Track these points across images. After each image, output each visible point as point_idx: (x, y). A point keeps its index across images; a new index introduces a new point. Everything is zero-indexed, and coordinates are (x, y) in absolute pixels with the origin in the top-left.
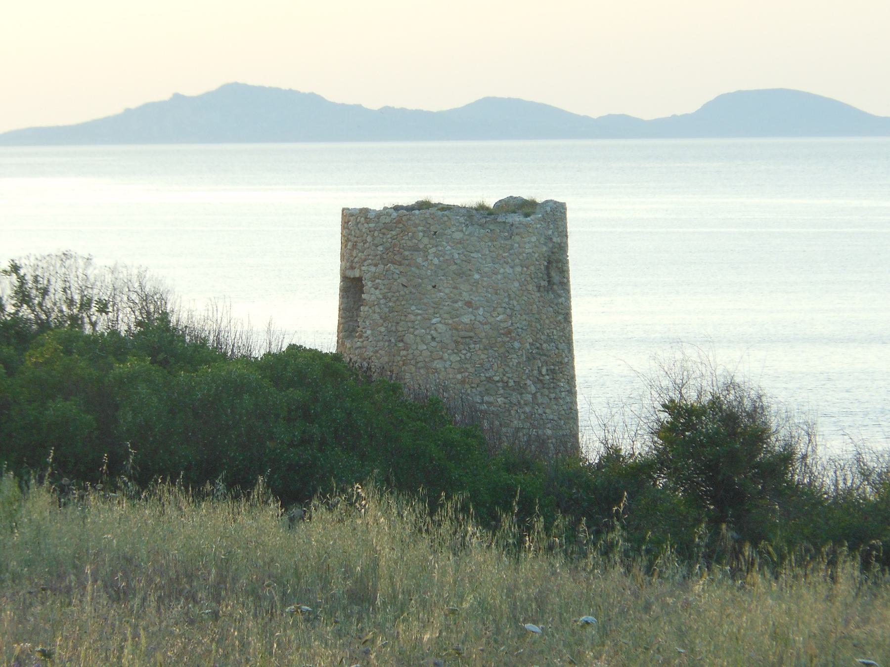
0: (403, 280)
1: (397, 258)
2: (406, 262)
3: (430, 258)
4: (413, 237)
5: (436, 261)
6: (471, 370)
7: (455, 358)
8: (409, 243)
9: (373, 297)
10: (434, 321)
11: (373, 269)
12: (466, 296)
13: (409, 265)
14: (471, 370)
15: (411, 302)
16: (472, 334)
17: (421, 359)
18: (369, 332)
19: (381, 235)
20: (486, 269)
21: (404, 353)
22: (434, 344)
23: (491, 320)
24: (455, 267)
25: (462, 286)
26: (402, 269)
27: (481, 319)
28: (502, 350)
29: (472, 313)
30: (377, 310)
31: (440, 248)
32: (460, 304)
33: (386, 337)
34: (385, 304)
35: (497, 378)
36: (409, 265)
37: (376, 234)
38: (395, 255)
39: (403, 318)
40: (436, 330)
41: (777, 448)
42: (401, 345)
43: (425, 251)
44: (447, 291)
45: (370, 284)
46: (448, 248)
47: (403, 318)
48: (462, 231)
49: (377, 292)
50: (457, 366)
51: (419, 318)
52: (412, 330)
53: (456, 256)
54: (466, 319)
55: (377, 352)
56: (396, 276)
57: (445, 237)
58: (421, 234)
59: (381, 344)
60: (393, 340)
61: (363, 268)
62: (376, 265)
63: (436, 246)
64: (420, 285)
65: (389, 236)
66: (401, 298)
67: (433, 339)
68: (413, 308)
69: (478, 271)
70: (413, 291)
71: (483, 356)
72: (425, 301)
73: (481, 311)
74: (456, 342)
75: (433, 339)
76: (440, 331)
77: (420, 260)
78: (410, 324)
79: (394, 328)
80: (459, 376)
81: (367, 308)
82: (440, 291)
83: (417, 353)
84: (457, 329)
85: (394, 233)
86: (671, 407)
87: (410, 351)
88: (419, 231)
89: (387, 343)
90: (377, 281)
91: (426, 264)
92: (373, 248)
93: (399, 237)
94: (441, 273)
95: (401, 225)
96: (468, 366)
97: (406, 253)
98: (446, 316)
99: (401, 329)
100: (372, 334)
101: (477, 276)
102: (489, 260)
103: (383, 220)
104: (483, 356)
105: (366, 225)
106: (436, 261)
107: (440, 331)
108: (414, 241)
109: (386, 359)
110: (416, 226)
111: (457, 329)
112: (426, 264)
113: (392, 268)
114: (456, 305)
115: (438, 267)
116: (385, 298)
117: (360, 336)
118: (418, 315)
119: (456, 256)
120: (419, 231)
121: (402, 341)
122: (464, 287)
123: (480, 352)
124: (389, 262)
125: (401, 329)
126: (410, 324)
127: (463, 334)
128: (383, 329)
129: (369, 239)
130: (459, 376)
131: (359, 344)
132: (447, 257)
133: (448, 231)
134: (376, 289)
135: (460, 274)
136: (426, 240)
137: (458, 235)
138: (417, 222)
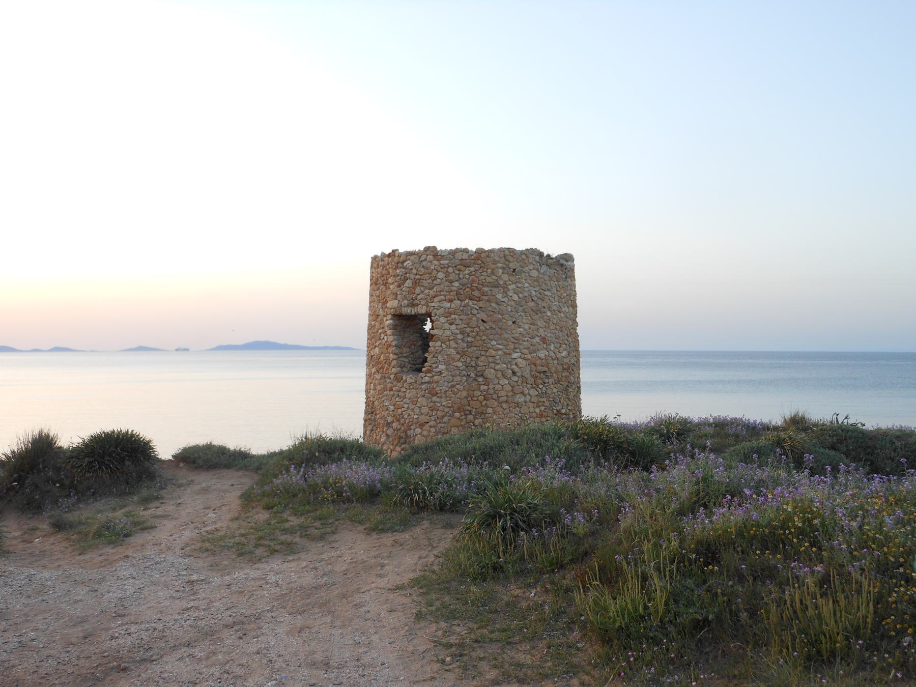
0: (483, 316)
1: (476, 293)
2: (486, 298)
3: (510, 294)
4: (493, 273)
5: (516, 298)
6: (547, 404)
7: (533, 392)
8: (489, 279)
9: (448, 333)
10: (515, 355)
11: (447, 305)
12: (542, 332)
13: (489, 301)
14: (547, 404)
15: (492, 337)
16: (546, 369)
17: (503, 393)
18: (442, 367)
19: (457, 272)
20: (555, 308)
21: (483, 387)
22: (515, 379)
23: (559, 355)
24: (532, 304)
25: (539, 323)
26: (481, 304)
27: (552, 354)
28: (565, 384)
29: (546, 349)
30: (453, 344)
31: (520, 285)
32: (537, 339)
33: (464, 372)
34: (462, 340)
35: (563, 411)
36: (489, 301)
37: (450, 270)
38: (473, 290)
39: (483, 353)
40: (516, 365)
41: (772, 587)
42: (480, 379)
43: (505, 288)
44: (527, 327)
45: (442, 320)
46: (527, 285)
47: (483, 353)
48: (538, 270)
49: (453, 327)
50: (535, 400)
51: (500, 352)
52: (493, 365)
53: (534, 293)
54: (542, 354)
55: (453, 386)
56: (475, 312)
57: (523, 274)
58: (501, 271)
59: (459, 378)
60: (473, 375)
61: (433, 304)
62: (451, 301)
63: (516, 283)
64: (500, 320)
65: (467, 272)
66: (481, 334)
67: (514, 373)
68: (494, 343)
69: (549, 309)
70: (494, 326)
71: (555, 390)
72: (506, 336)
73: (552, 347)
74: (535, 377)
75: (514, 373)
76: (520, 365)
77: (499, 296)
78: (490, 359)
79: (473, 364)
80: (538, 410)
81: (439, 343)
82: (520, 327)
83: (498, 387)
84: (535, 365)
85: (472, 269)
86: (40, 433)
87: (491, 386)
88: (498, 268)
89: (465, 378)
90: (453, 316)
91: (506, 300)
92: (447, 283)
93: (478, 274)
94: (521, 309)
95: (479, 262)
96: (544, 399)
97: (486, 289)
98: (525, 351)
99: (481, 364)
100: (447, 369)
101: (549, 314)
102: (556, 298)
103: (459, 256)
104: (555, 390)
105: (436, 262)
106: (516, 298)
107: (520, 365)
108: (494, 277)
109: (464, 393)
110: (495, 262)
111: (535, 365)
112: (506, 300)
113: (471, 303)
114: (534, 341)
115: (518, 303)
116: (462, 333)
117: (429, 371)
118: (499, 349)
119: (534, 293)
120: (498, 268)
121: (482, 375)
122: (541, 323)
123: (552, 386)
124: (466, 298)
125: (481, 364)
126: (490, 359)
127: (540, 368)
128: (460, 364)
129: (441, 275)
130: (538, 410)
131: (427, 379)
132: (526, 294)
133: (526, 269)
134: (451, 324)
135: (536, 312)
136: (505, 277)
137: (534, 273)
138: (497, 259)
